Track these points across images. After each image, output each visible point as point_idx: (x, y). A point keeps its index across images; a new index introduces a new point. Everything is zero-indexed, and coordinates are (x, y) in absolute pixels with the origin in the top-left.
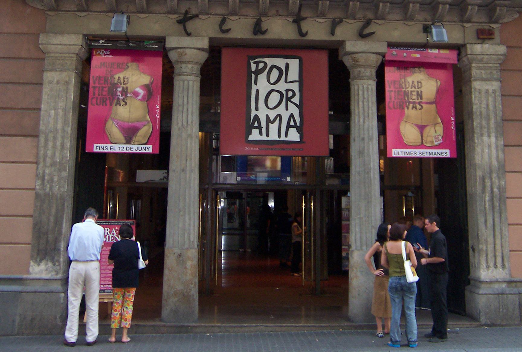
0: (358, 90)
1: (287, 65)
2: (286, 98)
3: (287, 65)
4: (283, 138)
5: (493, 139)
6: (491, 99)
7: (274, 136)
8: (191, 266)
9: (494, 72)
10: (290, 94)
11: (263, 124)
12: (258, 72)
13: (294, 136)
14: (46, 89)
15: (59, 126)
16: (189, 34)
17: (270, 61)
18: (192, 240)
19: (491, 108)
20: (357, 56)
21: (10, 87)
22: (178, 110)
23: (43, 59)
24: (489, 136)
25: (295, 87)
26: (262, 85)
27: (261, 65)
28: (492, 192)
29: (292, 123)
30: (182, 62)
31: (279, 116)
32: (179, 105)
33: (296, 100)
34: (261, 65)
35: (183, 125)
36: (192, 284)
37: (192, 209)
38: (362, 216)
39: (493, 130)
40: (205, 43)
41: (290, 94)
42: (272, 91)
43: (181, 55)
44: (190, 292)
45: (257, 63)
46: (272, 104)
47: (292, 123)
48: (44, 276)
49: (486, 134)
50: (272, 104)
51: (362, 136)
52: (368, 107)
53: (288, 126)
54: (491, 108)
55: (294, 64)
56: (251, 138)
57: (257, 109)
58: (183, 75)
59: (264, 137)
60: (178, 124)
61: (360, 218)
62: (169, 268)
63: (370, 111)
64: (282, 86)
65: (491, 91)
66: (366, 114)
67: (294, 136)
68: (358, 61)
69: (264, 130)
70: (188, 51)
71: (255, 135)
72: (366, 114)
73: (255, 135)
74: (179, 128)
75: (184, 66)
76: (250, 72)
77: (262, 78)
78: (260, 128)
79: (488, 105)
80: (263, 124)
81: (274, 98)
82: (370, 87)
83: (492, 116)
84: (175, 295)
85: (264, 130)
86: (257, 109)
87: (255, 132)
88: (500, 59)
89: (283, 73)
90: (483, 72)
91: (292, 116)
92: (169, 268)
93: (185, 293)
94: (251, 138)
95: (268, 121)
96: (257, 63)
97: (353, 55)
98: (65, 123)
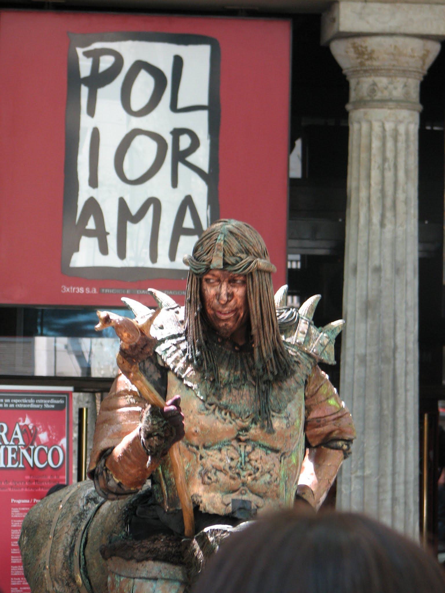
0: (370, 135)
2: (175, 153)
3: (178, 62)
10: (185, 142)
12: (99, 80)
17: (131, 51)
20: (371, 43)
25: (199, 123)
29: (188, 223)
33: (201, 158)
38: (368, 472)
41: (185, 142)
47: (188, 223)
52: (396, 183)
55: (198, 60)
57: (94, 182)
61: (363, 478)
64: (162, 120)
66: (389, 202)
68: (371, 58)
72: (389, 202)
77: (109, 96)
78: (101, 234)
86: (94, 182)
95: (125, 215)
96: (95, 56)
97: (358, 41)
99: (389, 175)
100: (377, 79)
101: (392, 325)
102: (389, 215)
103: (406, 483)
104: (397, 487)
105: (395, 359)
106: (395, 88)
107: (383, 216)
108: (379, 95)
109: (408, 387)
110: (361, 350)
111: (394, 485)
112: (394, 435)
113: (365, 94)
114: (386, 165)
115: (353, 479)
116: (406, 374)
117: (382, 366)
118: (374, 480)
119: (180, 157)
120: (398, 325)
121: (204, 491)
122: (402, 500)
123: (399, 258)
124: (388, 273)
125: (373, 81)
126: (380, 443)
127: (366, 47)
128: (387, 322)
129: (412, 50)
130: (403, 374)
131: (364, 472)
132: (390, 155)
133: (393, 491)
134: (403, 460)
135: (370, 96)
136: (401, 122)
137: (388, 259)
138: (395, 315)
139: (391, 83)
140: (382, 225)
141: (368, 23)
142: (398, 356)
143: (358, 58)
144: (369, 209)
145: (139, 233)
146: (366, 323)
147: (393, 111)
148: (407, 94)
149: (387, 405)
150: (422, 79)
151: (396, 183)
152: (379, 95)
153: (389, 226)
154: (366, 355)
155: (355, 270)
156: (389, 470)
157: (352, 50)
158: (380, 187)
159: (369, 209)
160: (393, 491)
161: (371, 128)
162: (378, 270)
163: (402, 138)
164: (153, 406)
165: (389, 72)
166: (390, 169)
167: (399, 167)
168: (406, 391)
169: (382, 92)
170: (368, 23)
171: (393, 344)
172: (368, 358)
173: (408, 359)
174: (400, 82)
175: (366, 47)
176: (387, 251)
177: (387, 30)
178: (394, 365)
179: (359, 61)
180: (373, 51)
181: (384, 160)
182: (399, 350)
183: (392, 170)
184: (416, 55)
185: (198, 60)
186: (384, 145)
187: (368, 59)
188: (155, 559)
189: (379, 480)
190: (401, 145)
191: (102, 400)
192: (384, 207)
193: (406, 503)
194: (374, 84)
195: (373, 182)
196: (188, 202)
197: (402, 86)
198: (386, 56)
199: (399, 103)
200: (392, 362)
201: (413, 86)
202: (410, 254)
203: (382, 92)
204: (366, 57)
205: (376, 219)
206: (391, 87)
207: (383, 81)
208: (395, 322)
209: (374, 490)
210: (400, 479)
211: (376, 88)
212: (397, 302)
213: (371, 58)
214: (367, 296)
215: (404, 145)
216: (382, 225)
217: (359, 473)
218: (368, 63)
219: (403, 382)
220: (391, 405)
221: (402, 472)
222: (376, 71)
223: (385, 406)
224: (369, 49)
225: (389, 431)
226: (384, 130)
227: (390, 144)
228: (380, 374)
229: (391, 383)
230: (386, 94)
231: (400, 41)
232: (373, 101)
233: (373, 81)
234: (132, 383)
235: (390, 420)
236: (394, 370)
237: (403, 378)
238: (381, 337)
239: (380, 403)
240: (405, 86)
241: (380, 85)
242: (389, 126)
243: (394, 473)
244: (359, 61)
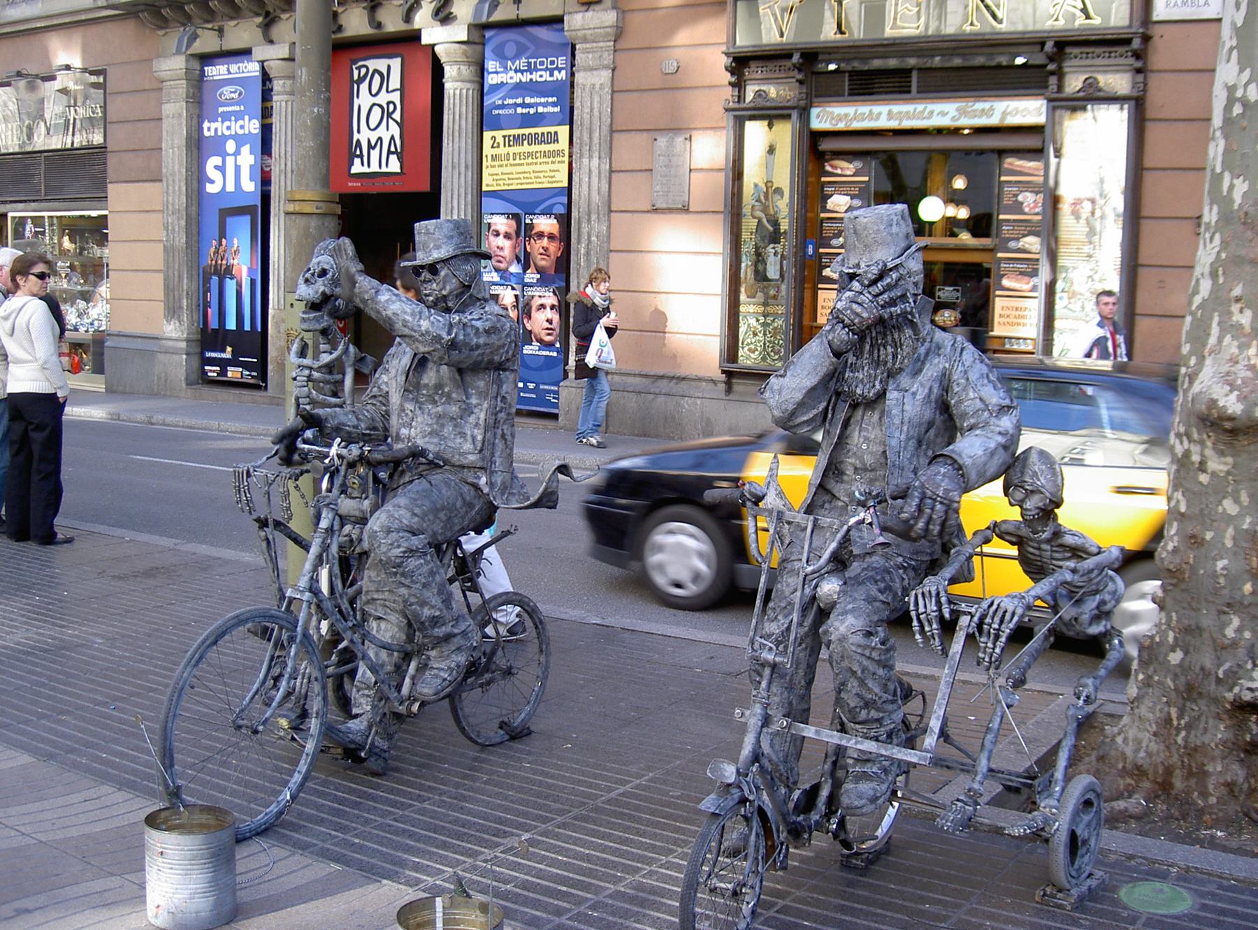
1: (389, 67)
2: (387, 114)
3: (389, 67)
4: (384, 169)
5: (595, 162)
6: (596, 99)
7: (374, 168)
9: (605, 54)
10: (391, 107)
11: (365, 153)
12: (361, 80)
13: (394, 166)
14: (165, 124)
15: (177, 167)
16: (271, 42)
17: (373, 64)
19: (596, 113)
21: (140, 124)
23: (161, 89)
24: (591, 157)
25: (396, 97)
26: (363, 100)
27: (363, 71)
28: (589, 242)
29: (393, 149)
31: (380, 139)
33: (397, 116)
34: (363, 71)
39: (596, 148)
41: (391, 107)
42: (374, 104)
45: (359, 68)
46: (373, 124)
47: (393, 149)
48: (174, 335)
49: (586, 154)
50: (373, 124)
53: (389, 152)
54: (596, 113)
55: (396, 64)
56: (354, 170)
57: (359, 131)
59: (365, 169)
64: (383, 98)
65: (598, 86)
67: (394, 166)
71: (357, 168)
73: (357, 168)
76: (352, 81)
77: (364, 87)
78: (361, 156)
79: (592, 110)
80: (365, 153)
81: (377, 112)
83: (596, 123)
86: (359, 131)
87: (357, 161)
88: (608, 34)
89: (385, 78)
90: (590, 56)
91: (392, 137)
94: (354, 170)
95: (370, 147)
96: (359, 68)
98: (180, 164)
119: (390, 115)
121: (457, 225)
145: (375, 154)
164: (103, 147)
185: (396, 64)
188: (123, 785)
196: (392, 137)
234: (1049, 630)
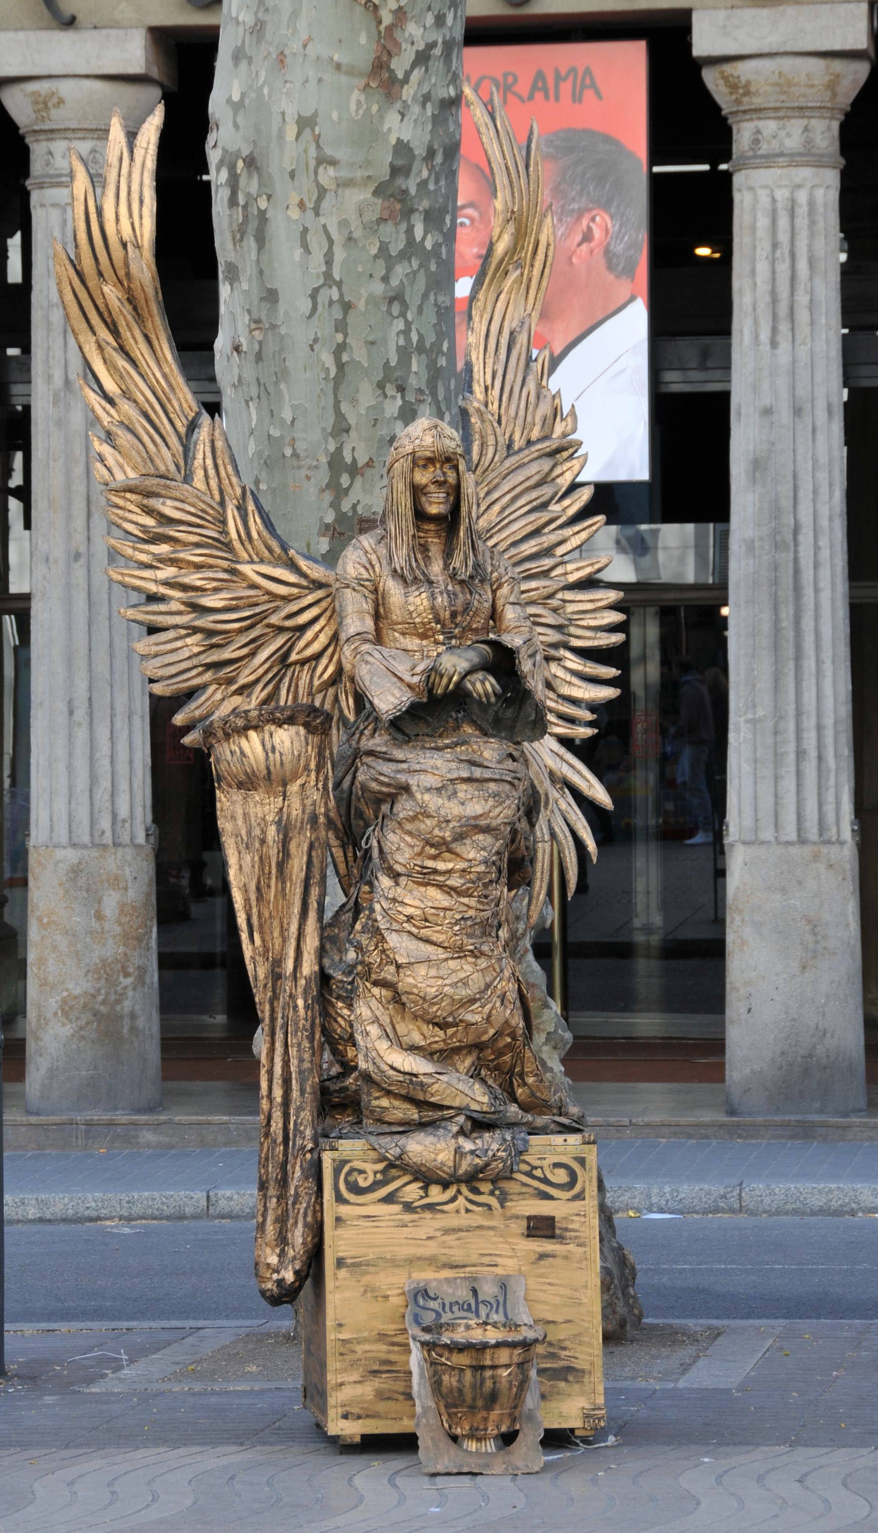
0: (754, 210)
8: (122, 908)
11: (551, 83)
16: (70, 23)
18: (123, 811)
20: (743, 70)
22: (49, 323)
30: (52, 133)
32: (51, 306)
35: (67, 382)
36: (127, 975)
37: (121, 701)
38: (760, 713)
40: (133, 53)
43: (43, 105)
44: (118, 1001)
51: (767, 401)
52: (793, 279)
58: (54, 185)
60: (49, 379)
61: (754, 722)
62: (40, 920)
63: (803, 299)
66: (783, 309)
68: (747, 93)
69: (551, 93)
70: (65, 88)
72: (783, 309)
74: (56, 396)
75: (59, 146)
80: (551, 83)
82: (802, 197)
84: (65, 1014)
85: (551, 93)
92: (40, 920)
93: (104, 1009)
97: (728, 68)
99: (783, 268)
100: (761, 124)
101: (791, 493)
102: (784, 328)
103: (819, 728)
104: (805, 735)
105: (796, 543)
106: (789, 135)
107: (774, 330)
108: (764, 148)
109: (822, 584)
110: (749, 533)
111: (799, 731)
112: (798, 658)
113: (747, 148)
114: (778, 254)
115: (742, 724)
116: (816, 566)
117: (777, 556)
118: (770, 724)
120: (801, 493)
122: (813, 753)
123: (800, 392)
124: (784, 415)
125: (756, 127)
126: (776, 670)
127: (739, 77)
128: (786, 489)
129: (808, 75)
130: (811, 566)
131: (755, 713)
132: (784, 237)
133: (799, 739)
134: (814, 694)
135: (753, 149)
136: (799, 186)
137: (784, 394)
138: (795, 478)
139: (784, 128)
140: (774, 344)
141: (736, 40)
142: (801, 538)
143: (731, 94)
144: (756, 322)
146: (754, 492)
147: (786, 171)
148: (808, 142)
149: (787, 613)
150: (843, 118)
151: (793, 279)
152: (764, 148)
153: (784, 346)
154: (753, 541)
155: (739, 414)
156: (791, 710)
157: (721, 82)
158: (770, 287)
159: (756, 322)
160: (799, 739)
161: (756, 200)
162: (767, 412)
163: (802, 211)
165: (779, 112)
166: (784, 260)
167: (798, 255)
168: (817, 590)
169: (769, 142)
170: (736, 40)
171: (792, 521)
172: (757, 544)
173: (821, 543)
174: (796, 126)
175: (739, 77)
176: (782, 383)
177: (766, 50)
178: (796, 552)
179: (734, 97)
180: (748, 83)
181: (775, 246)
182: (804, 530)
183: (788, 260)
184: (816, 82)
186: (774, 222)
187: (744, 95)
189: (776, 723)
190: (802, 222)
191: (750, 1114)
192: (775, 316)
193: (820, 758)
194: (758, 132)
195: (759, 281)
197: (800, 130)
198: (768, 88)
199: (795, 159)
200: (792, 549)
201: (825, 134)
202: (830, 391)
203: (769, 142)
204: (741, 91)
205: (765, 336)
206: (782, 133)
207: (769, 126)
208: (796, 489)
209: (770, 740)
210: (810, 722)
211: (760, 137)
212: (799, 458)
213: (747, 93)
214: (754, 451)
215: (806, 221)
216: (774, 344)
217: (750, 716)
218: (745, 99)
219: (811, 578)
220: (791, 612)
221: (814, 712)
222: (758, 112)
223: (783, 615)
224: (743, 80)
225: (790, 652)
226: (774, 200)
227: (783, 222)
228: (776, 567)
229: (791, 580)
230: (775, 144)
231: (787, 63)
232: (756, 157)
233: (756, 127)
235: (790, 635)
236: (796, 560)
237: (812, 572)
238: (776, 512)
239: (776, 609)
240: (806, 129)
241: (765, 133)
242: (781, 195)
243: (799, 714)
244: (734, 97)
